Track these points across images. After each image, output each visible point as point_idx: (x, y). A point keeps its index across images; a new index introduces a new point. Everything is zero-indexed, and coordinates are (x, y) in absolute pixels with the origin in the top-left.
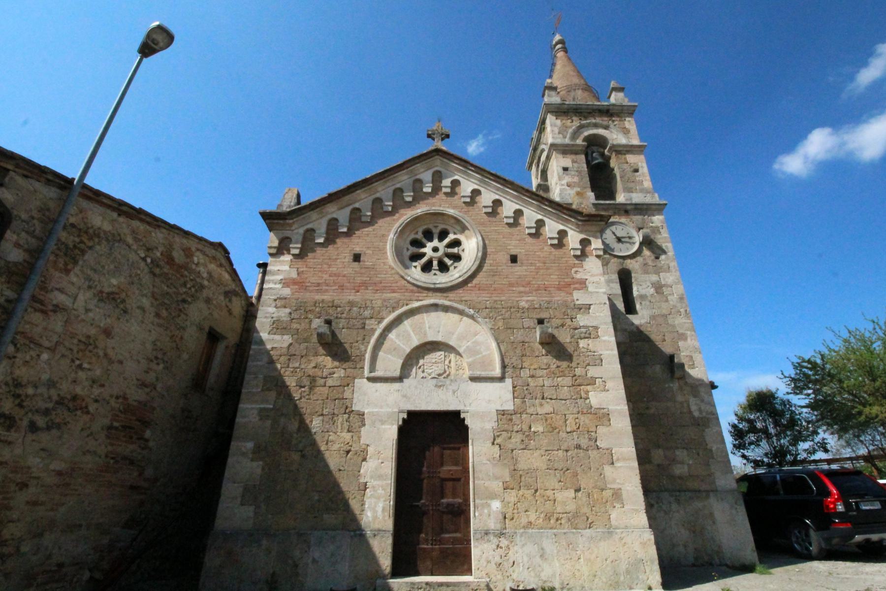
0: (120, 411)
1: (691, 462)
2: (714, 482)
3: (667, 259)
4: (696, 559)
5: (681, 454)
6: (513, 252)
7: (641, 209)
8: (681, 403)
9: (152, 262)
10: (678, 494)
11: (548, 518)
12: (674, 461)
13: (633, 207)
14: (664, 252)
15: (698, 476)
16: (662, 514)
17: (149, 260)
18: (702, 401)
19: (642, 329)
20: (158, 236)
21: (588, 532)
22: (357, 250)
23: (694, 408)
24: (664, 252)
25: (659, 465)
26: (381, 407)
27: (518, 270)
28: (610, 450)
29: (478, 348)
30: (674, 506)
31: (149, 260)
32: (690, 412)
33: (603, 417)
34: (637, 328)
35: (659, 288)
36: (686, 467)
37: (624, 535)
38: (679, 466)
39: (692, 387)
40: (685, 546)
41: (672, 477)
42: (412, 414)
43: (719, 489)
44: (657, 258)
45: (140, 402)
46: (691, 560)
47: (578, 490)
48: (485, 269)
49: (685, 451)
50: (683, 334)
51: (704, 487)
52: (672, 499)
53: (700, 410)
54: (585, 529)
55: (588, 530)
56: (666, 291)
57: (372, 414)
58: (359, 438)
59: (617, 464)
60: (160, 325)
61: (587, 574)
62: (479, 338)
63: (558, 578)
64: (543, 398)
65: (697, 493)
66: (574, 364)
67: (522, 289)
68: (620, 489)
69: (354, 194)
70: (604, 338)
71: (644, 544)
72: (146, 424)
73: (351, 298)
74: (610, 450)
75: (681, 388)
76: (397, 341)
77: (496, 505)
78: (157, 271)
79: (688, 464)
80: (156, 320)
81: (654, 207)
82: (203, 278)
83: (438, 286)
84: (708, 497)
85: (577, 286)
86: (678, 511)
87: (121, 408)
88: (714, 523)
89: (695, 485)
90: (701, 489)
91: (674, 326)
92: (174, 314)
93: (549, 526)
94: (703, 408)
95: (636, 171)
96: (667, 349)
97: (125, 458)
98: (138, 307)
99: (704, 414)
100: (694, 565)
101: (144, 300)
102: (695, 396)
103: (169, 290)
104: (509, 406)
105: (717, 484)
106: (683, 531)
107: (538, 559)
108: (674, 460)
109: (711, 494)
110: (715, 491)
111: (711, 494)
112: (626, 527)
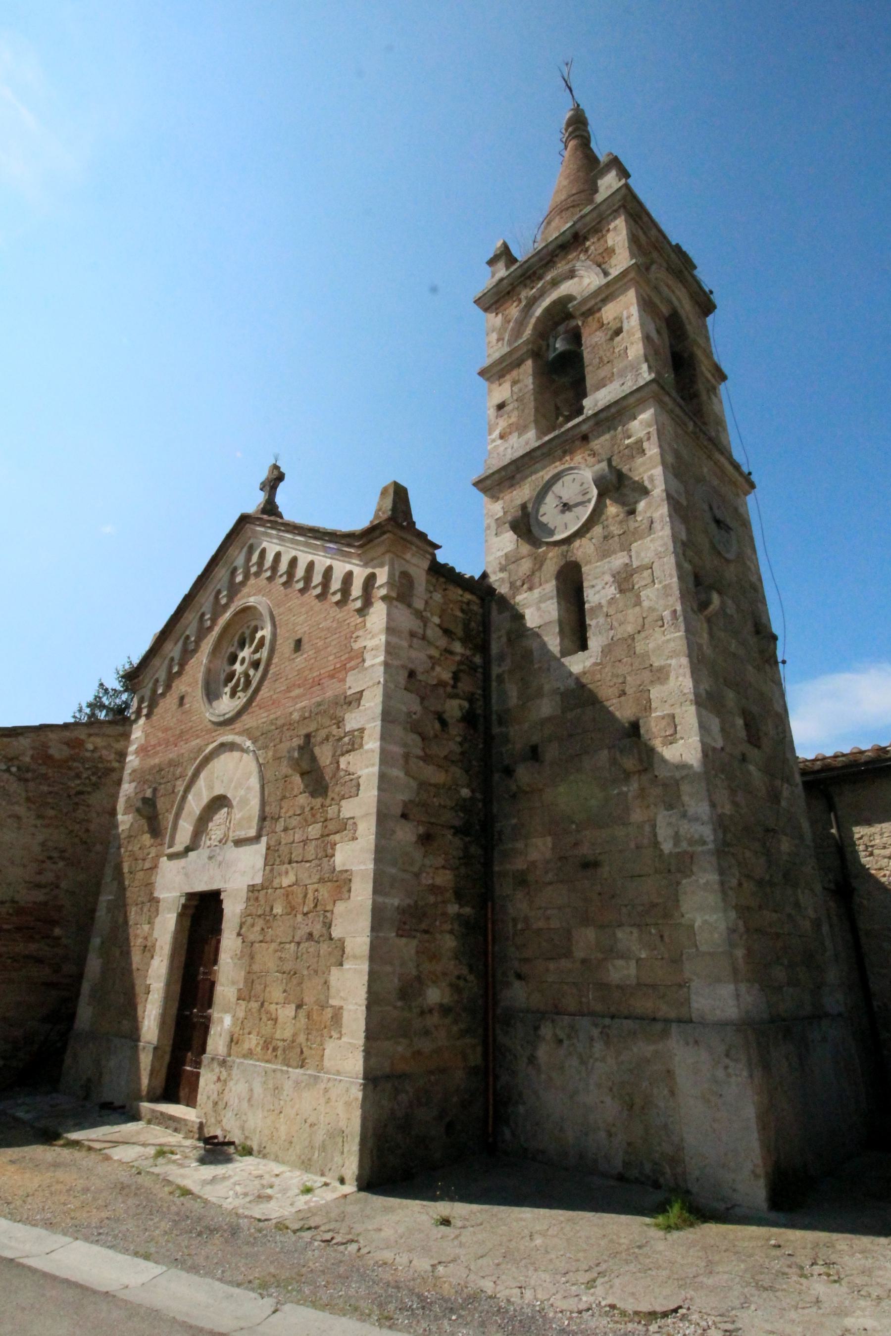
0: (11, 915)
1: (643, 956)
2: (688, 1000)
3: (649, 505)
4: (626, 1164)
5: (628, 938)
7: (607, 419)
8: (640, 826)
9: (19, 768)
10: (607, 1021)
11: (266, 1047)
12: (611, 952)
13: (591, 423)
14: (645, 492)
15: (654, 987)
16: (575, 1062)
17: (14, 769)
18: (684, 815)
19: (584, 680)
20: (24, 742)
21: (296, 1073)
23: (664, 833)
24: (645, 492)
25: (584, 961)
28: (342, 941)
30: (598, 1048)
31: (14, 769)
32: (656, 844)
33: (341, 884)
34: (577, 679)
36: (633, 963)
37: (330, 1084)
38: (620, 963)
39: (665, 785)
40: (610, 1135)
41: (603, 986)
42: (190, 896)
43: (694, 1016)
44: (632, 512)
45: (35, 903)
46: (618, 1164)
47: (299, 1007)
48: (269, 676)
49: (635, 931)
50: (661, 669)
51: (665, 1010)
52: (595, 1032)
53: (677, 838)
54: (297, 1068)
55: (298, 1071)
57: (164, 898)
59: (346, 966)
60: (47, 826)
61: (283, 1138)
63: (257, 1136)
64: (290, 862)
65: (654, 1025)
66: (328, 802)
68: (341, 1008)
69: (182, 620)
71: (348, 1104)
72: (54, 923)
74: (342, 941)
75: (642, 793)
78: (29, 775)
79: (638, 960)
80: (39, 822)
81: (632, 400)
82: (110, 761)
83: (227, 716)
84: (665, 1034)
86: (603, 1060)
87: (11, 911)
88: (672, 1093)
89: (644, 1005)
90: (659, 1015)
91: (646, 655)
92: (65, 810)
93: (266, 1058)
94: (682, 832)
96: (624, 712)
97: (27, 957)
98: (9, 817)
99: (684, 845)
100: (621, 1178)
101: (17, 808)
102: (670, 807)
103: (51, 789)
104: (258, 880)
105: (694, 1005)
106: (608, 1100)
107: (245, 1104)
108: (611, 950)
109: (674, 1027)
110: (685, 1021)
111: (674, 1027)
112: (338, 1073)
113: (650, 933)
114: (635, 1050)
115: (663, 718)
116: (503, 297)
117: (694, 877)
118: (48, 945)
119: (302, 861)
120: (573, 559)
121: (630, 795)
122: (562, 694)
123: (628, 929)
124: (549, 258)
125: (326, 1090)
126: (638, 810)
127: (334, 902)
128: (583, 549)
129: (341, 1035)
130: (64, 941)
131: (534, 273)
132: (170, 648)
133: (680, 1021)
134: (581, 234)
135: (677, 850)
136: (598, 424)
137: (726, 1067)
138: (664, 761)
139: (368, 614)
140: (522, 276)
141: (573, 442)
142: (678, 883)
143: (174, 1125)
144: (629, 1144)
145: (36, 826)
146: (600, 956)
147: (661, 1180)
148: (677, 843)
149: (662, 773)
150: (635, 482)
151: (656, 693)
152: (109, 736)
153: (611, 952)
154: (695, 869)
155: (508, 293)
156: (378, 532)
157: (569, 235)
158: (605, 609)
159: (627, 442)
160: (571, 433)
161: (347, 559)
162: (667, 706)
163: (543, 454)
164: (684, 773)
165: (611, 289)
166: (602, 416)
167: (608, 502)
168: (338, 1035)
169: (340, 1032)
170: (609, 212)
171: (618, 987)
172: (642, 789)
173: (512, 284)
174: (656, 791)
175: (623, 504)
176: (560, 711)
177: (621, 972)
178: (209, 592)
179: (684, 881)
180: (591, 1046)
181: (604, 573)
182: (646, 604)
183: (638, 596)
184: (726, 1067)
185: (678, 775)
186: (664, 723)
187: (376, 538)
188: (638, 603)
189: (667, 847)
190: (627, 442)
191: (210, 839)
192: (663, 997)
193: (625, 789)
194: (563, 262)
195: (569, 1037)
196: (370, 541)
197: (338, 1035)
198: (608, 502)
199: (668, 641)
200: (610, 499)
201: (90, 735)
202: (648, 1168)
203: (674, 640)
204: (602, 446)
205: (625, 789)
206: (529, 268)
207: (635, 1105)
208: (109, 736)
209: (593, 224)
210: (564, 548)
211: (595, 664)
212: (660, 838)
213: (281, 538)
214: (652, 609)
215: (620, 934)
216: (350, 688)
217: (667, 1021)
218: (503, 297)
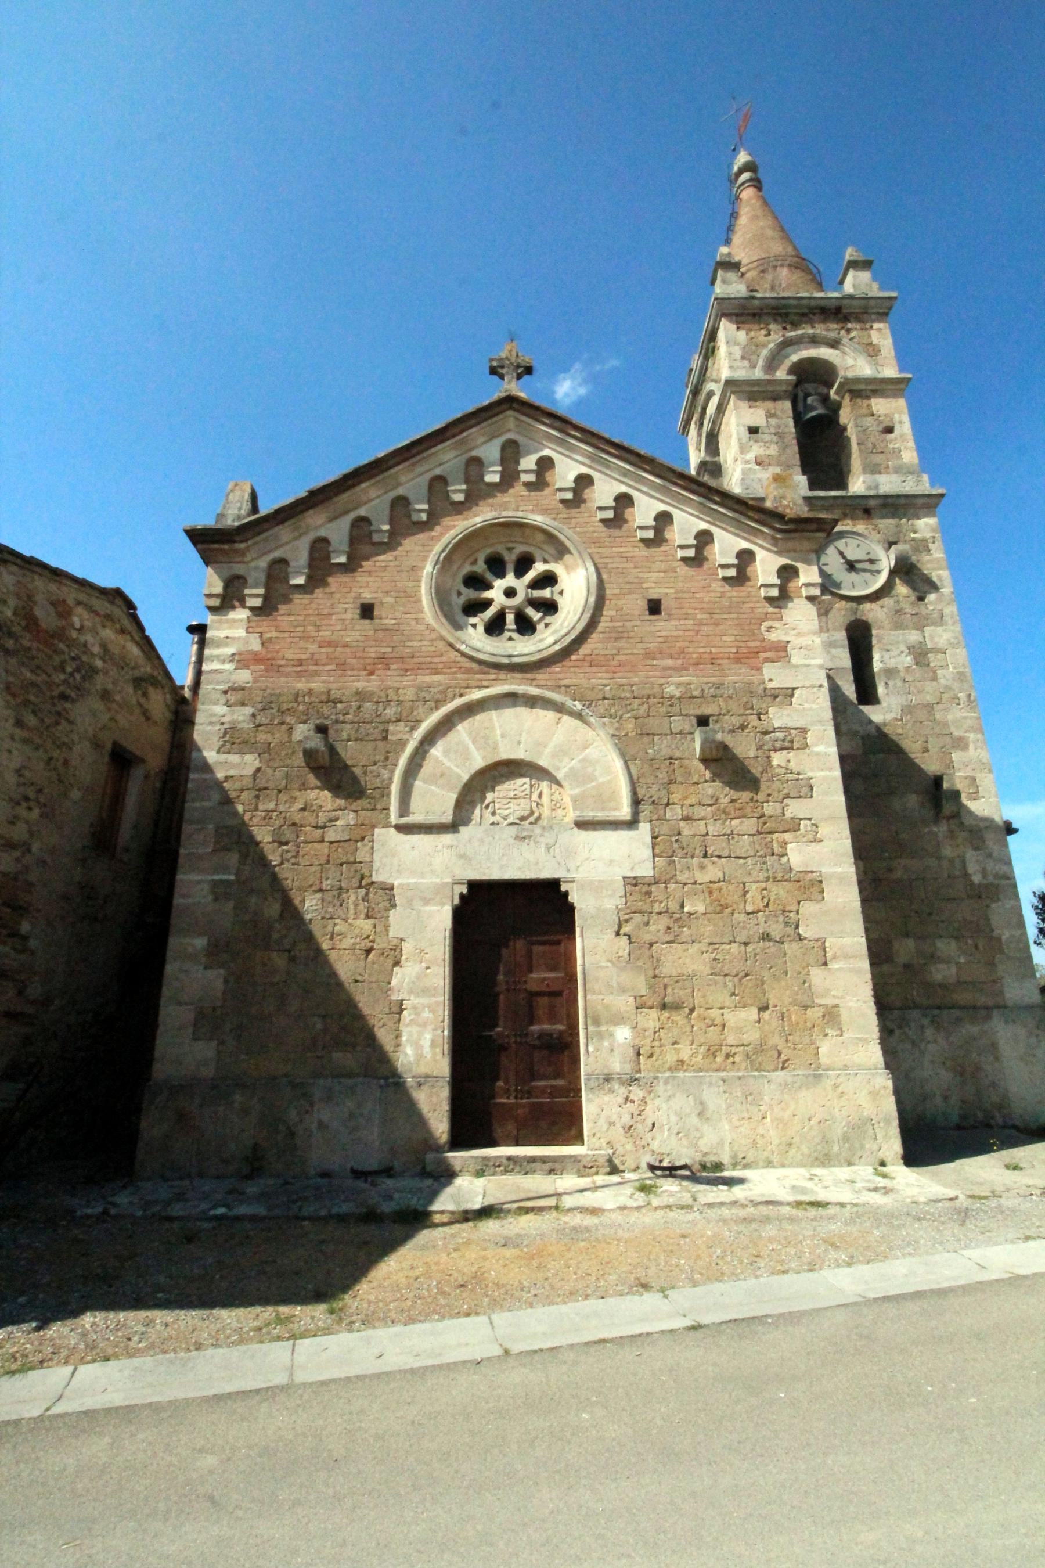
4: (963, 1117)
5: (946, 947)
6: (654, 595)
8: (951, 861)
10: (936, 1012)
11: (712, 1053)
12: (933, 958)
18: (990, 855)
19: (886, 730)
22: (367, 596)
23: (972, 868)
25: (907, 966)
26: (422, 875)
27: (661, 626)
29: (590, 770)
30: (929, 1033)
32: (966, 875)
34: (878, 728)
35: (920, 654)
40: (946, 1098)
44: (921, 599)
46: (955, 1118)
50: (960, 739)
51: (982, 1000)
52: (926, 1022)
53: (984, 872)
55: (779, 1073)
56: (934, 660)
58: (387, 927)
59: (834, 965)
62: (592, 752)
64: (705, 856)
65: (979, 1012)
66: (761, 797)
67: (669, 662)
70: (816, 749)
73: (360, 685)
76: (445, 761)
77: (623, 1034)
79: (958, 963)
80: (18, 732)
81: (920, 501)
84: (988, 1018)
85: (769, 654)
88: (997, 1059)
89: (963, 997)
91: (946, 725)
94: (989, 868)
95: (889, 430)
96: (931, 766)
99: (991, 879)
100: (959, 1127)
105: (1008, 996)
107: (694, 1120)
113: (966, 944)
114: (964, 1031)
115: (966, 778)
116: (748, 314)
117: (1000, 903)
118: (14, 949)
119: (729, 857)
120: (864, 618)
121: (940, 835)
122: (863, 738)
123: (945, 941)
124: (806, 311)
125: (836, 1086)
126: (949, 848)
127: (799, 902)
128: (874, 613)
129: (842, 1032)
130: (33, 943)
131: (787, 315)
132: (319, 522)
133: (998, 1007)
134: (844, 311)
135: (985, 882)
136: (884, 506)
137: (1037, 1036)
138: (970, 812)
139: (786, 607)
140: (773, 308)
141: (855, 509)
142: (988, 906)
143: (547, 1166)
144: (963, 1102)
145: (12, 738)
146: (922, 961)
147: (993, 1122)
148: (984, 876)
149: (968, 821)
150: (924, 574)
151: (956, 756)
152: (97, 613)
153: (933, 958)
154: (1001, 896)
155: (754, 315)
156: (814, 526)
157: (835, 303)
158: (902, 674)
159: (912, 535)
160: (858, 501)
161: (752, 538)
162: (969, 769)
163: (823, 506)
164: (987, 824)
165: (884, 386)
166: (890, 501)
167: (898, 581)
168: (839, 1032)
169: (841, 1029)
170: (874, 311)
171: (940, 985)
172: (951, 831)
173: (762, 309)
174: (962, 835)
175: (914, 589)
176: (861, 752)
177: (941, 973)
178: (419, 469)
179: (994, 906)
180: (923, 1033)
181: (898, 642)
182: (943, 681)
183: (935, 672)
184: (1037, 1036)
185: (982, 825)
186: (967, 782)
187: (807, 531)
188: (935, 679)
189: (977, 879)
190: (912, 535)
191: (494, 814)
192: (981, 990)
193: (935, 829)
194: (822, 326)
195: (900, 1027)
196: (795, 531)
197: (839, 1032)
198: (898, 581)
199: (965, 718)
200: (900, 579)
201: (79, 603)
202: (980, 1115)
203: (971, 718)
204: (887, 528)
205: (935, 829)
206: (785, 307)
207: (966, 1071)
208: (97, 613)
209: (857, 311)
210: (854, 605)
211: (896, 719)
212: (970, 871)
213: (592, 458)
214: (948, 688)
215: (940, 944)
216: (771, 680)
217: (988, 1008)
218: (748, 314)
